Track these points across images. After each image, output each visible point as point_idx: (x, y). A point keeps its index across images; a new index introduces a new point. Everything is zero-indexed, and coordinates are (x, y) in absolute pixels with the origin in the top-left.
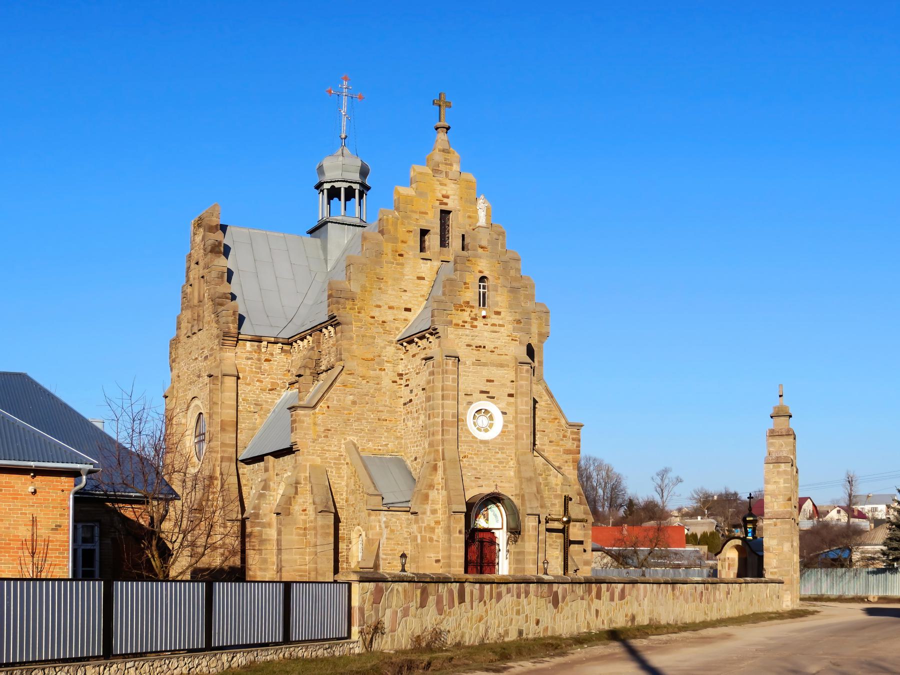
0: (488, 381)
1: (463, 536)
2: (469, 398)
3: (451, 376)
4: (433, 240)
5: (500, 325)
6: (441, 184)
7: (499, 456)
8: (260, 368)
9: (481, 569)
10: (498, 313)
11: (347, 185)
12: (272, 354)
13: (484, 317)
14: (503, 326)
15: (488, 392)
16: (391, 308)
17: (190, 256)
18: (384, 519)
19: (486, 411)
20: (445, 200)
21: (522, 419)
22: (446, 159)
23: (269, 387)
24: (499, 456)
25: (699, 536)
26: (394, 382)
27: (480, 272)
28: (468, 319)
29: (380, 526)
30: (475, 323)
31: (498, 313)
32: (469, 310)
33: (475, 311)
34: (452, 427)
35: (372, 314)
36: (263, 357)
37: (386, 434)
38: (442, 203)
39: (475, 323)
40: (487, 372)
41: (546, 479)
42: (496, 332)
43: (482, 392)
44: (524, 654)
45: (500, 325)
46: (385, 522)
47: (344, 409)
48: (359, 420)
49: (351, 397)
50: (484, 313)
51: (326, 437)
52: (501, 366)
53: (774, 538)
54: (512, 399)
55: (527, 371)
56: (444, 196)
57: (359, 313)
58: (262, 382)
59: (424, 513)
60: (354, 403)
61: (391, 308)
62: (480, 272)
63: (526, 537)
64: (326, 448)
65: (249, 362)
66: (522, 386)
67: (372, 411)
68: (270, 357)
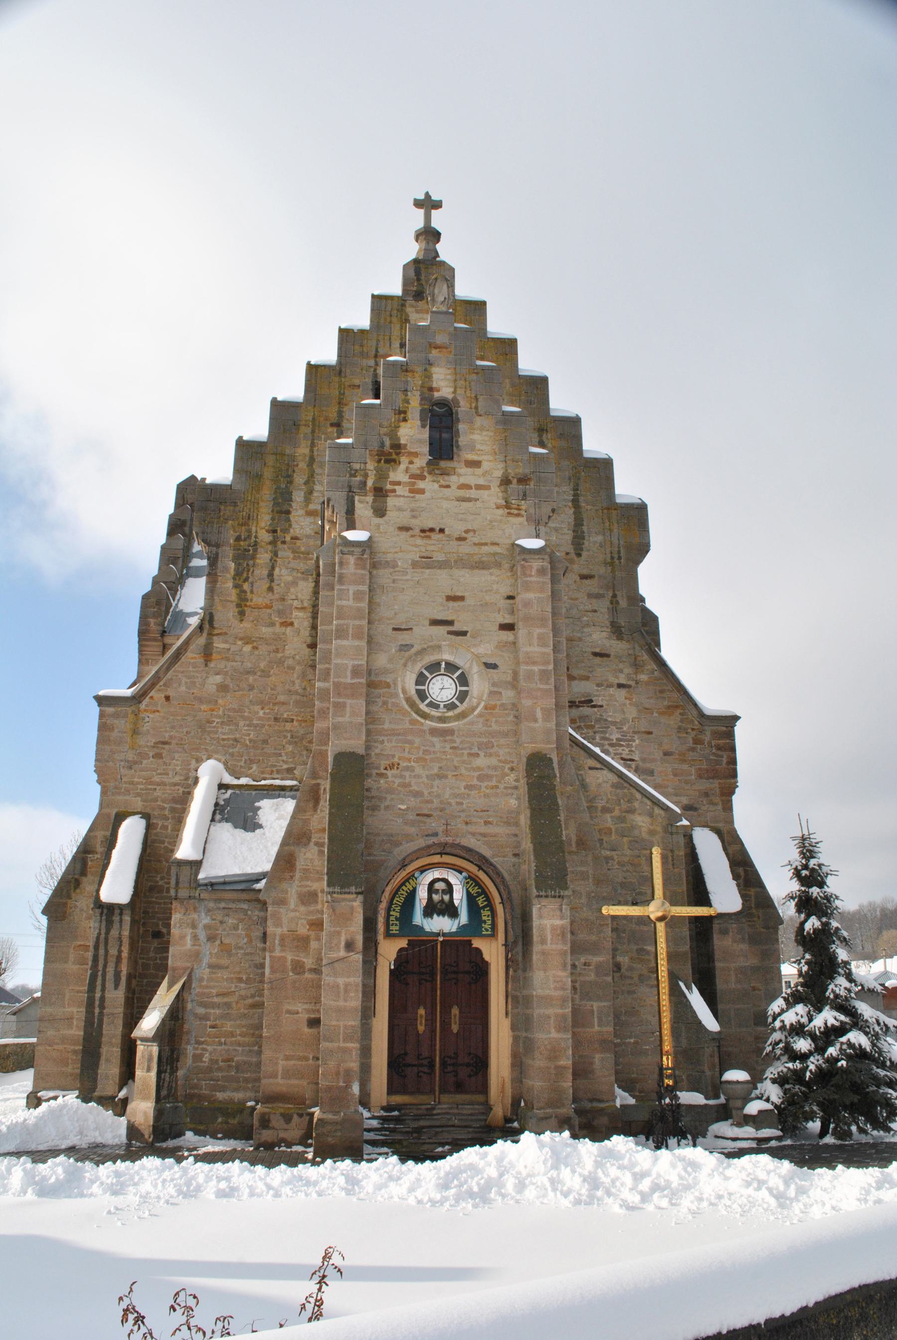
0: (450, 598)
3: (352, 589)
5: (479, 487)
7: (481, 762)
10: (476, 464)
14: (487, 488)
15: (450, 623)
18: (206, 920)
21: (530, 676)
24: (481, 762)
25: (438, 259)
29: (195, 937)
30: (421, 485)
31: (476, 464)
34: (353, 696)
37: (290, 748)
40: (444, 581)
41: (621, 819)
42: (469, 500)
43: (435, 622)
45: (479, 487)
46: (206, 927)
47: (200, 700)
48: (230, 721)
49: (218, 679)
51: (158, 756)
52: (481, 565)
54: (507, 636)
55: (541, 572)
59: (282, 902)
60: (223, 688)
64: (156, 779)
66: (527, 604)
67: (262, 704)
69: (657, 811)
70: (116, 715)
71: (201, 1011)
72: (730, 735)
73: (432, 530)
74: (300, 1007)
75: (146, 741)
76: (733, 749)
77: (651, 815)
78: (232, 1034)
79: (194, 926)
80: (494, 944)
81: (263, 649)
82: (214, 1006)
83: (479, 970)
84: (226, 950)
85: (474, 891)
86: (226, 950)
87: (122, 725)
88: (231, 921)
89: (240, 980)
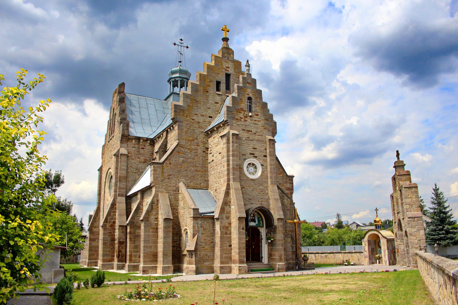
0: (254, 148)
1: (244, 231)
2: (244, 157)
4: (223, 86)
5: (258, 121)
6: (226, 62)
8: (139, 152)
9: (435, 240)
10: (257, 115)
11: (181, 79)
12: (145, 146)
13: (251, 116)
15: (253, 154)
16: (202, 116)
17: (111, 107)
18: (200, 222)
19: (253, 164)
20: (228, 69)
22: (227, 52)
23: (143, 161)
24: (261, 187)
26: (204, 152)
27: (248, 95)
28: (243, 117)
29: (198, 226)
30: (246, 119)
32: (243, 112)
33: (246, 113)
34: (237, 171)
35: (193, 118)
36: (141, 147)
38: (226, 70)
39: (246, 119)
43: (251, 154)
44: (138, 244)
45: (258, 121)
46: (200, 224)
49: (182, 159)
50: (250, 114)
51: (169, 178)
53: (414, 228)
56: (227, 67)
57: (186, 117)
58: (139, 158)
60: (183, 162)
61: (202, 116)
62: (248, 95)
63: (277, 231)
64: (169, 185)
65: (134, 149)
68: (144, 147)
69: (289, 199)
70: (158, 167)
71: (200, 244)
72: (292, 180)
73: (249, 131)
74: (227, 243)
75: (166, 175)
76: (293, 184)
77: (287, 200)
78: (207, 249)
79: (198, 224)
80: (263, 228)
81: (193, 152)
82: (203, 242)
83: (258, 233)
84: (205, 229)
85: (259, 216)
86: (205, 229)
87: (159, 170)
88: (205, 223)
89: (208, 236)
